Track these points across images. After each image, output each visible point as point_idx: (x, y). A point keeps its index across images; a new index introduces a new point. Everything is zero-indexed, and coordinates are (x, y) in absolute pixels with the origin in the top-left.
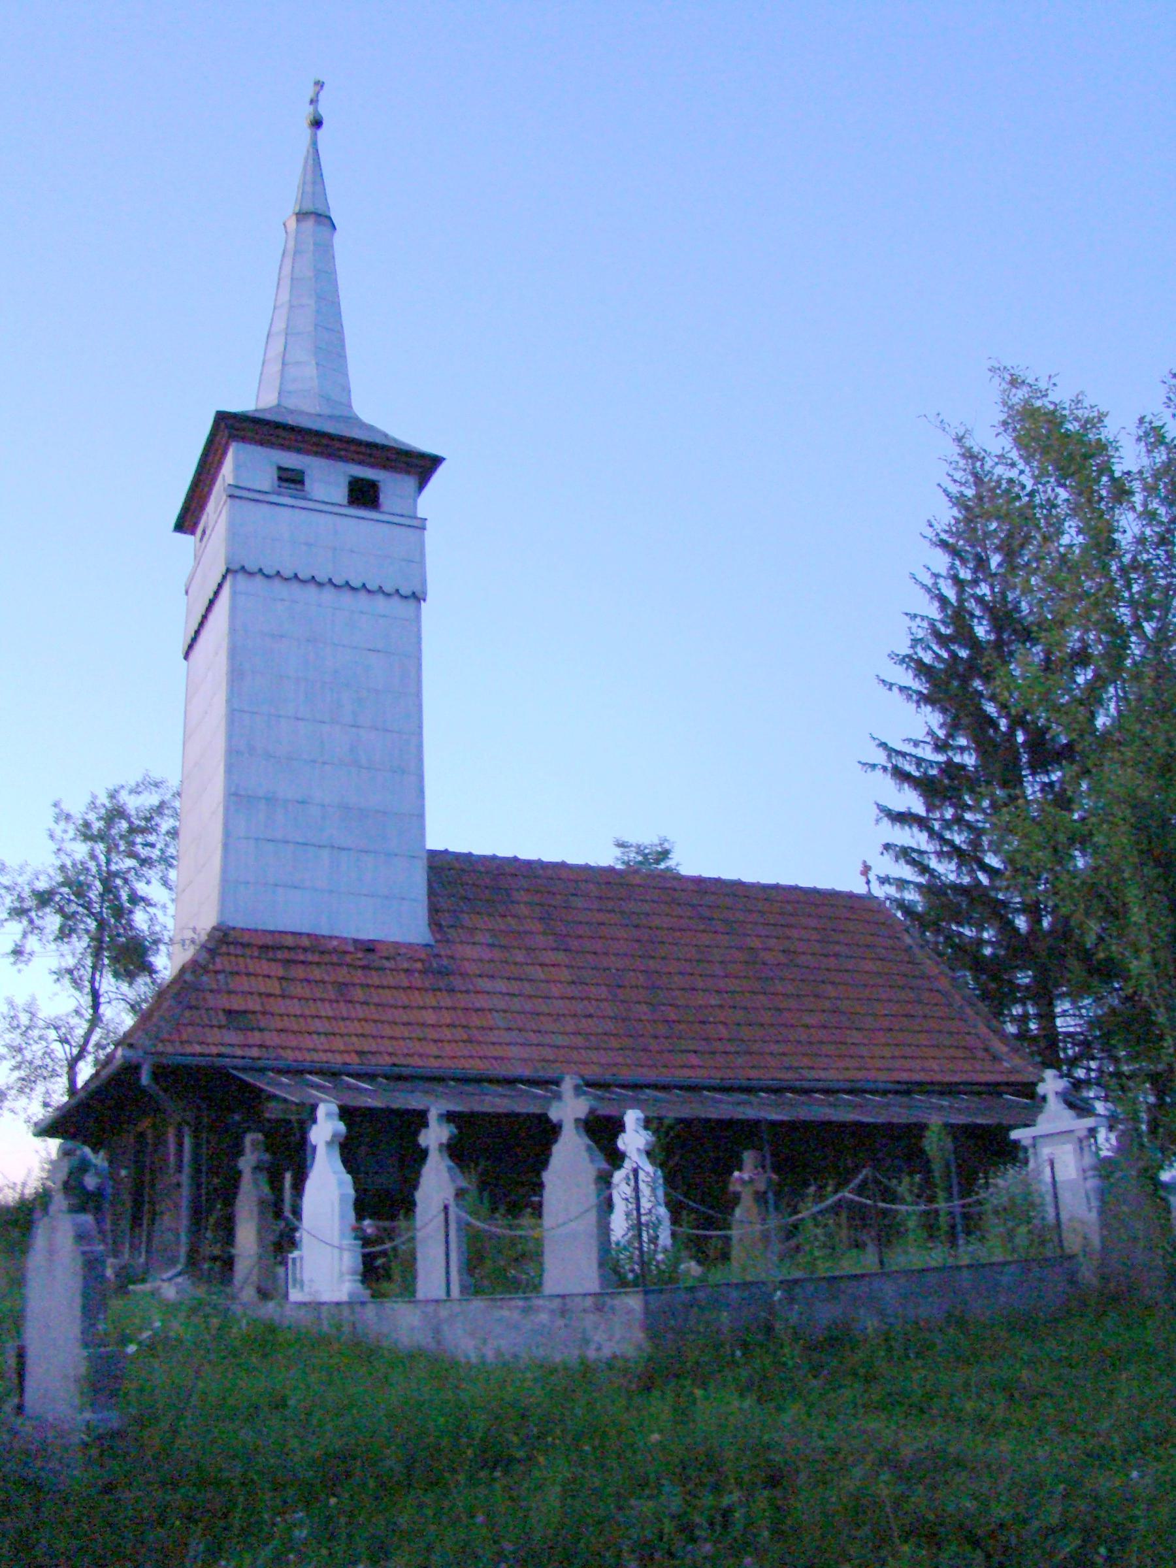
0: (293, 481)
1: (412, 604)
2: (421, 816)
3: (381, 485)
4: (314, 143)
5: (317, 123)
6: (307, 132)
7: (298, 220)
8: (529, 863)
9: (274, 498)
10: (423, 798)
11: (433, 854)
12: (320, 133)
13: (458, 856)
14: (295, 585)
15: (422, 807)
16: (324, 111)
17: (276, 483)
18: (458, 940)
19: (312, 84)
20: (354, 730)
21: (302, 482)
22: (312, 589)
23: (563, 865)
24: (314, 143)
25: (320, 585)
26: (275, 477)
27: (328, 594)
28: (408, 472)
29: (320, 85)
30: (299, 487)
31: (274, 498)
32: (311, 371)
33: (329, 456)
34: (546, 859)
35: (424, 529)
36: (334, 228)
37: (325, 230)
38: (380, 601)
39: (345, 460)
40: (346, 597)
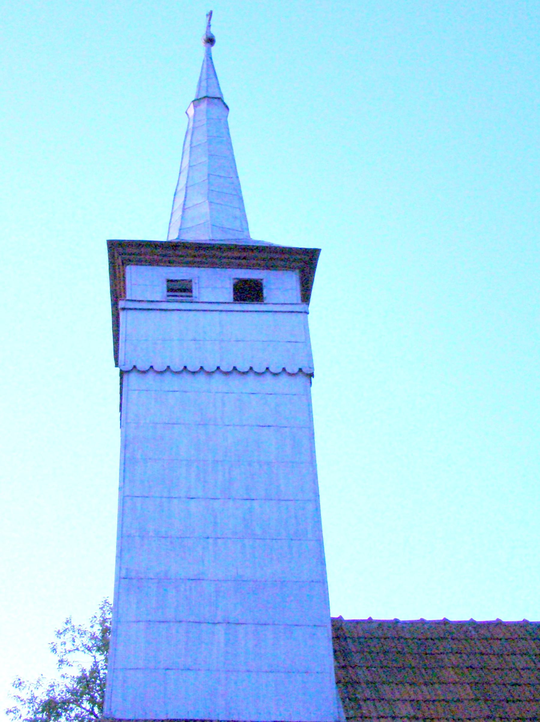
0: (185, 290)
1: (301, 380)
2: (323, 582)
3: (264, 283)
4: (209, 58)
5: (210, 41)
6: (202, 47)
7: (195, 107)
8: (460, 624)
9: (164, 306)
10: (323, 563)
11: (333, 619)
12: (214, 49)
13: (381, 624)
14: (187, 377)
15: (324, 573)
16: (214, 31)
17: (166, 293)
18: (374, 714)
19: (205, 16)
20: (247, 502)
21: (191, 291)
22: (202, 378)
23: (498, 623)
24: (209, 58)
25: (210, 373)
26: (165, 290)
27: (218, 381)
28: (285, 268)
29: (210, 15)
30: (188, 294)
31: (164, 306)
32: (205, 209)
33: (213, 265)
34: (479, 618)
35: (307, 313)
36: (227, 108)
37: (217, 111)
38: (269, 381)
39: (229, 266)
40: (235, 382)
